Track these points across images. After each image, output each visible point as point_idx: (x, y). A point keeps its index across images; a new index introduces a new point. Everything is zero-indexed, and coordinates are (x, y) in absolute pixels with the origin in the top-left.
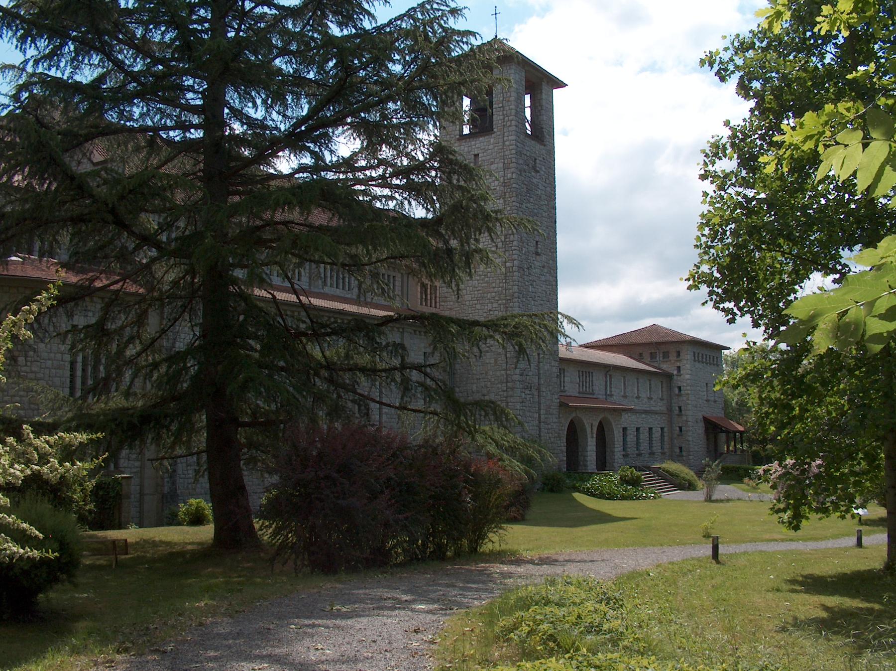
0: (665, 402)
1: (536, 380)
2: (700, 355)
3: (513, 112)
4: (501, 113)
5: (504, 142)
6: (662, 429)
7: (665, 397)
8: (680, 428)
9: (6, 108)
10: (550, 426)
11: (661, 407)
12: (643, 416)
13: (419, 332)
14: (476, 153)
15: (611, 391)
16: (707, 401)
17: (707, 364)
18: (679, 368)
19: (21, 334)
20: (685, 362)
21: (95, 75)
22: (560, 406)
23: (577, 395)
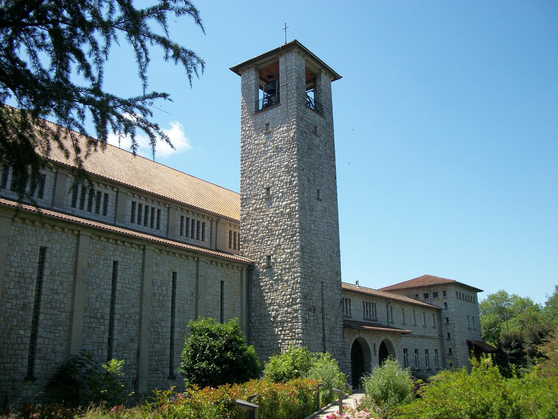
0: (437, 330)
1: (320, 304)
2: (461, 294)
3: (295, 87)
4: (285, 89)
5: (288, 111)
6: (436, 350)
7: (437, 326)
8: (450, 349)
9: (122, 117)
10: (334, 345)
11: (435, 333)
12: (420, 340)
13: (233, 266)
14: (267, 122)
15: (392, 320)
16: (469, 329)
17: (467, 301)
18: (446, 304)
19: (108, 413)
20: (450, 299)
22: (344, 327)
23: (363, 321)
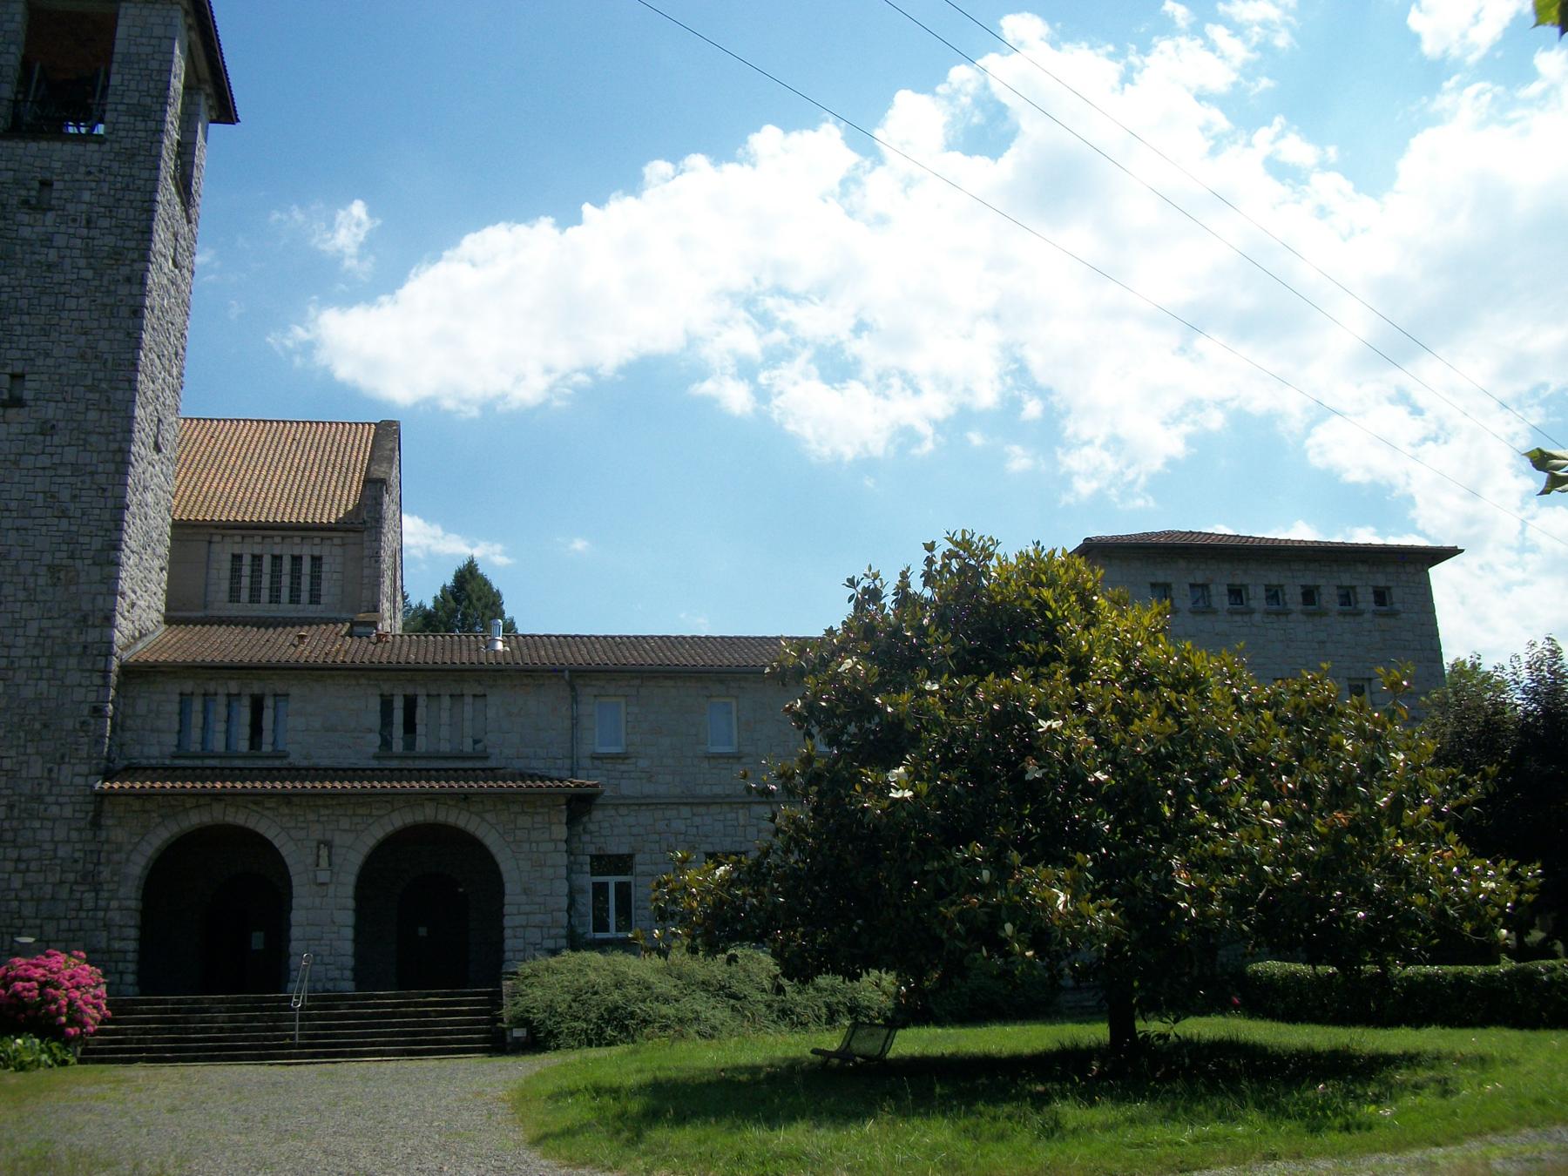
14: (18, 370)
21: (1446, 666)
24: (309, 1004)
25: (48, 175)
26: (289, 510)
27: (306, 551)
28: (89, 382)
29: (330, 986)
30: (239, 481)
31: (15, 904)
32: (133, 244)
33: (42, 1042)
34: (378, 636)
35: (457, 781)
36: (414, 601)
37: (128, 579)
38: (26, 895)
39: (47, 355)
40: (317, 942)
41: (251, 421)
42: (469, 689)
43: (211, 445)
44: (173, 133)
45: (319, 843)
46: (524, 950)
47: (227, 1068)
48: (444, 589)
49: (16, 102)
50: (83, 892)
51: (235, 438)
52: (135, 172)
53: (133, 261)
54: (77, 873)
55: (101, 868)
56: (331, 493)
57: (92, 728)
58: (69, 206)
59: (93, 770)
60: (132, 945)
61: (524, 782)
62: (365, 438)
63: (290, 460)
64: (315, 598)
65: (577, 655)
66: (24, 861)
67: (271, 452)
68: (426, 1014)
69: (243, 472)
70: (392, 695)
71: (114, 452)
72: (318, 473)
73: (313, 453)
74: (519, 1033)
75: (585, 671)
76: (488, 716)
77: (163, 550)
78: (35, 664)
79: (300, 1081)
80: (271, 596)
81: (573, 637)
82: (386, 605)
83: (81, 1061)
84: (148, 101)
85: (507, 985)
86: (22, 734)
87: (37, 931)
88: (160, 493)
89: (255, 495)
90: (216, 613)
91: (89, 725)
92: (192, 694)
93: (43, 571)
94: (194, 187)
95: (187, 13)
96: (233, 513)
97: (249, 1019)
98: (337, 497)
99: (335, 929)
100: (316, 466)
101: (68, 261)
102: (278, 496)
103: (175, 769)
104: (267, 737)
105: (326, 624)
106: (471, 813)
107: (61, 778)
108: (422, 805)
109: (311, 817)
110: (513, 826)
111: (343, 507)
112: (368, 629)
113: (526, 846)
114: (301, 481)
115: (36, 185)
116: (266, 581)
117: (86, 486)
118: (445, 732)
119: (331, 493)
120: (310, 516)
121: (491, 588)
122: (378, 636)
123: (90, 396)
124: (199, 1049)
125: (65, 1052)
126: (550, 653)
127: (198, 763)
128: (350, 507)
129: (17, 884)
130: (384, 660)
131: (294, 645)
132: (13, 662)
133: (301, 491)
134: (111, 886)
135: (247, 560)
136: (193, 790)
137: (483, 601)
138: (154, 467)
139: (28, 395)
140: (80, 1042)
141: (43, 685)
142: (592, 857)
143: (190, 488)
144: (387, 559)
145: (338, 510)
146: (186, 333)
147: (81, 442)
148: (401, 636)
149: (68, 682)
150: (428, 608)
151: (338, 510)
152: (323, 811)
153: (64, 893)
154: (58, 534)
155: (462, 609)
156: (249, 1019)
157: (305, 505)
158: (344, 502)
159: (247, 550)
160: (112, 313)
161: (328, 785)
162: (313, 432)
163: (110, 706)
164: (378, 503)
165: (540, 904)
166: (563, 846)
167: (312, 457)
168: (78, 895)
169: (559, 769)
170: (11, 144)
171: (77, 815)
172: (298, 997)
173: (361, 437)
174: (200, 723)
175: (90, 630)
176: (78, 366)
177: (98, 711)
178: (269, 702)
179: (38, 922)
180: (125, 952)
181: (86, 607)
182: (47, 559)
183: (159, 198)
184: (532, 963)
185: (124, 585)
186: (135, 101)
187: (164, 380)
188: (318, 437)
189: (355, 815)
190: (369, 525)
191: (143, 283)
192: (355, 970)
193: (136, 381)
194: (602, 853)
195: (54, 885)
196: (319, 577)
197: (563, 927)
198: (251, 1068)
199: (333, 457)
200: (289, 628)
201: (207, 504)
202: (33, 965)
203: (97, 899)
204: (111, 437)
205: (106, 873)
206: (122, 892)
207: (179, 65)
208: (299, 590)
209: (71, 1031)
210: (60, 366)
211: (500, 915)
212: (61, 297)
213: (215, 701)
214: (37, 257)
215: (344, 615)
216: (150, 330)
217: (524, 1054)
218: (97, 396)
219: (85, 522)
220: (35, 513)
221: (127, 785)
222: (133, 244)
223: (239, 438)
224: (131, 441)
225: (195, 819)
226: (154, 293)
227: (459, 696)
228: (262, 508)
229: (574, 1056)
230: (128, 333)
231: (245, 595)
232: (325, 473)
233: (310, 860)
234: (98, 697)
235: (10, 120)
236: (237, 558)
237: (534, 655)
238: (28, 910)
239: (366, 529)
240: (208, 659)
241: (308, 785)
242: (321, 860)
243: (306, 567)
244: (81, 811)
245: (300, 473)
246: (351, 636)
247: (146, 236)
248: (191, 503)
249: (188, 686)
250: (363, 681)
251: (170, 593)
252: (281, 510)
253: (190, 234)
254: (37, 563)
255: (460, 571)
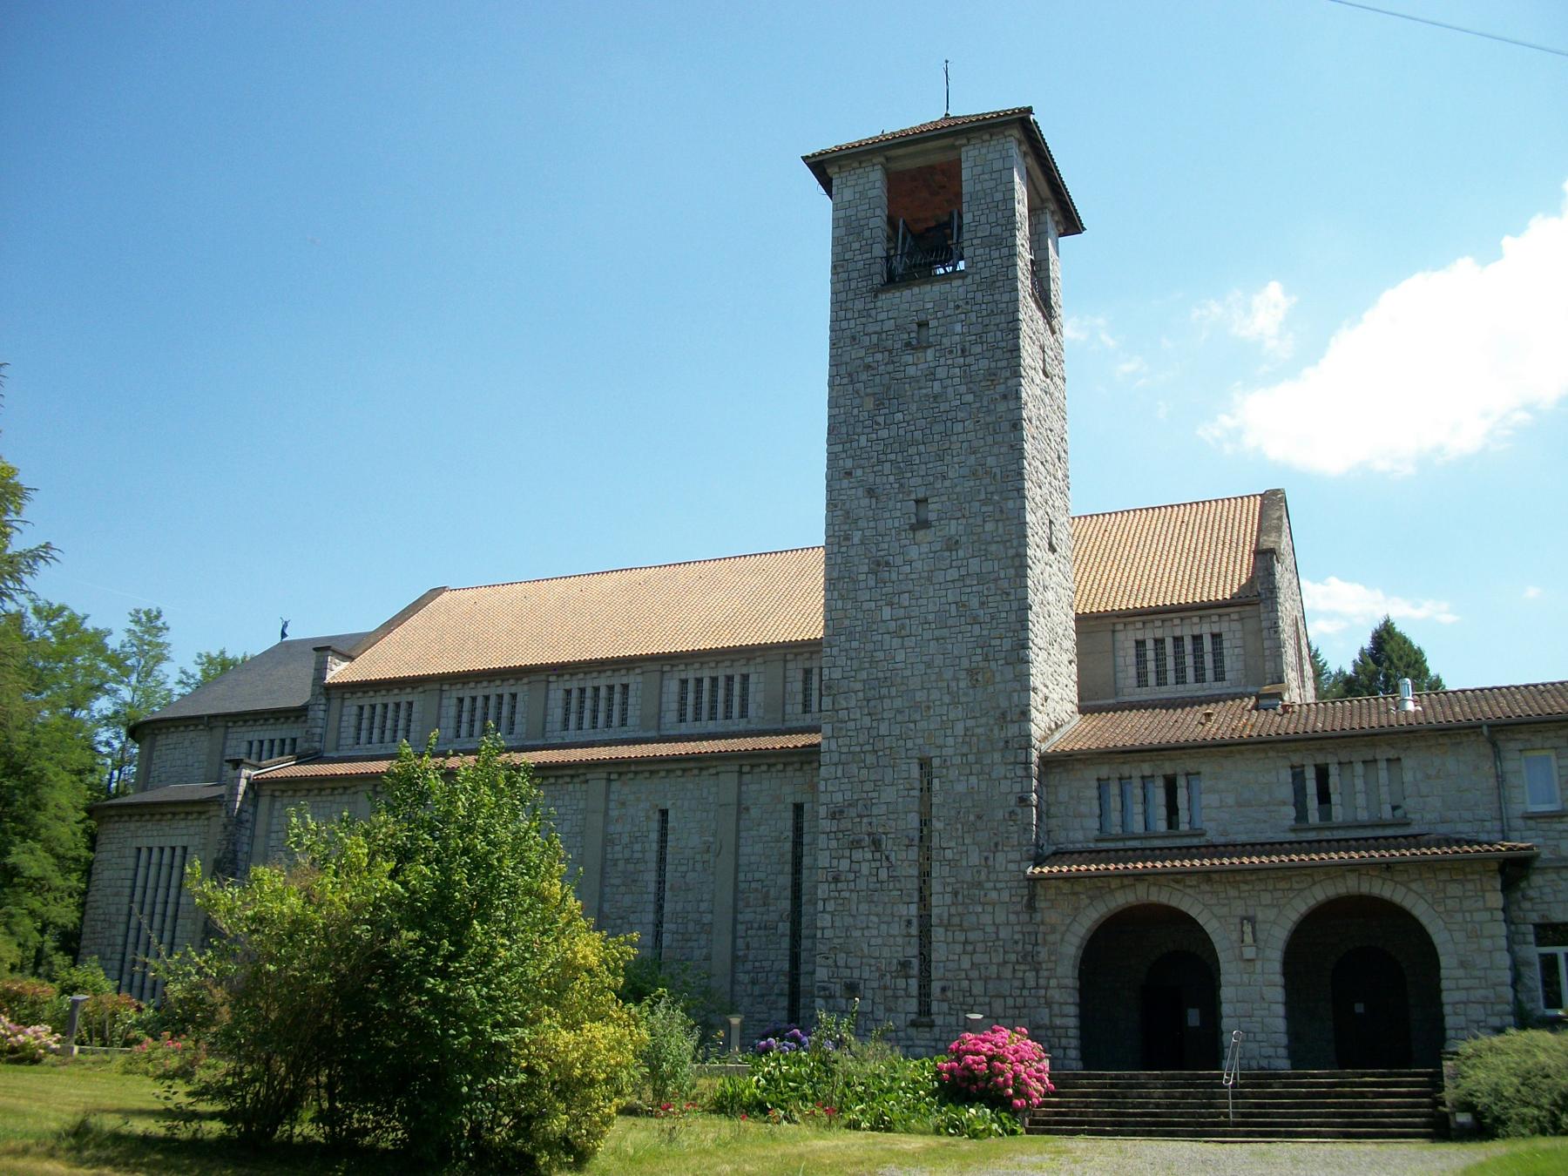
14: (921, 496)
24: (1242, 1082)
25: (922, 317)
26: (1184, 592)
27: (1206, 630)
28: (983, 496)
29: (1264, 1063)
30: (1134, 569)
31: (965, 984)
32: (1004, 364)
33: (992, 1112)
34: (1284, 707)
35: (1377, 850)
36: (1333, 668)
37: (1039, 675)
38: (974, 974)
39: (944, 478)
40: (1248, 1019)
41: (1141, 510)
42: (1383, 753)
43: (1106, 538)
44: (1025, 255)
45: (1243, 919)
46: (1467, 1028)
47: (1163, 1144)
48: (1362, 652)
49: (888, 259)
50: (1024, 972)
51: (1127, 528)
52: (997, 297)
53: (1007, 378)
54: (1017, 954)
55: (1039, 948)
56: (1223, 569)
57: (1020, 817)
58: (945, 340)
59: (1024, 857)
60: (1072, 1022)
61: (1418, 849)
62: (1251, 510)
63: (1181, 543)
64: (1219, 676)
65: (1496, 709)
66: (971, 943)
67: (1163, 537)
68: (1362, 1095)
69: (1137, 560)
70: (1303, 766)
71: (1013, 557)
72: (1209, 551)
73: (1202, 532)
74: (1463, 1118)
75: (1506, 725)
76: (1405, 780)
77: (1070, 644)
78: (964, 761)
79: (1230, 1159)
80: (1177, 677)
81: (1490, 690)
82: (1291, 676)
83: (1029, 1132)
84: (998, 230)
85: (1448, 1066)
86: (959, 826)
87: (987, 1008)
88: (1060, 590)
89: (1151, 581)
90: (1127, 699)
91: (1016, 814)
92: (1109, 779)
93: (963, 675)
94: (1053, 299)
95: (1020, 143)
96: (1132, 601)
97: (1184, 1096)
98: (1230, 573)
99: (1266, 1005)
100: (1207, 544)
101: (950, 390)
102: (1173, 579)
103: (1099, 852)
104: (1183, 815)
105: (1233, 700)
106: (1396, 883)
107: (997, 866)
108: (1343, 876)
109: (1233, 893)
110: (1442, 895)
111: (1236, 582)
112: (1274, 701)
113: (1459, 917)
114: (1193, 562)
115: (915, 327)
116: (1170, 663)
117: (992, 592)
118: (1361, 800)
119: (1223, 569)
120: (1205, 594)
121: (1411, 646)
122: (1284, 707)
123: (984, 509)
124: (1137, 1124)
125: (1013, 1122)
126: (1466, 708)
127: (1120, 845)
128: (1244, 581)
129: (966, 964)
130: (1291, 731)
131: (1202, 724)
132: (945, 760)
133: (1195, 571)
134: (1051, 965)
135: (1150, 645)
136: (1117, 872)
137: (1405, 660)
138: (1051, 566)
139: (932, 516)
140: (1027, 1113)
141: (973, 779)
142: (1536, 926)
143: (1090, 582)
144: (1286, 628)
145: (1232, 586)
146: (1065, 436)
147: (983, 553)
148: (1316, 704)
149: (994, 775)
150: (1348, 673)
151: (1232, 586)
152: (1244, 887)
153: (1007, 973)
154: (972, 639)
155: (1384, 671)
156: (1184, 1096)
157: (1200, 585)
158: (1237, 577)
159: (1149, 635)
160: (995, 430)
161: (1246, 860)
162: (1200, 513)
163: (1034, 795)
164: (1270, 573)
165: (1480, 978)
166: (1500, 915)
167: (1202, 536)
168: (1020, 975)
169: (1488, 832)
170: (889, 295)
171: (1014, 899)
172: (1229, 1075)
173: (1248, 510)
174: (1119, 806)
175: (1009, 726)
176: (972, 483)
177: (1023, 801)
178: (1181, 782)
179: (987, 1000)
180: (1067, 1028)
181: (1004, 704)
182: (965, 663)
183: (1021, 317)
184: (1474, 1042)
185: (1035, 681)
186: (988, 233)
187: (1050, 484)
188: (1205, 516)
189: (1276, 890)
190: (1264, 597)
191: (1019, 398)
192: (1287, 1047)
193: (1024, 489)
194: (1546, 921)
195: (999, 965)
196: (1221, 654)
197: (1508, 1003)
198: (1186, 1144)
199: (1222, 534)
200: (1197, 707)
201: (1106, 595)
202: (980, 1039)
203: (1038, 978)
204: (1008, 544)
205: (1043, 955)
206: (1060, 971)
207: (1021, 191)
208: (1203, 669)
209: (1018, 1102)
210: (956, 486)
211: (1438, 991)
212: (949, 424)
213: (1130, 783)
214: (924, 391)
215: (1250, 689)
216: (1030, 439)
217: (1469, 1141)
218: (991, 508)
219: (994, 625)
220: (950, 622)
221: (1055, 869)
222: (1004, 364)
223: (1130, 528)
224: (1026, 545)
225: (1122, 899)
226: (1029, 405)
227: (1371, 761)
228: (1158, 593)
229: (1521, 1147)
230: (1012, 446)
231: (1152, 678)
232: (1216, 550)
233: (1235, 936)
234: (1022, 788)
235: (885, 276)
236: (1140, 644)
237: (1449, 712)
238: (978, 988)
239: (1261, 601)
240: (1120, 744)
241: (1226, 861)
242: (1245, 936)
243: (1207, 645)
244: (1016, 895)
245: (1192, 554)
246: (1257, 709)
247: (1015, 354)
248: (1092, 596)
249: (1104, 771)
250: (1271, 754)
251: (1081, 684)
252: (1177, 593)
253: (1057, 344)
254: (957, 668)
255: (1377, 632)
